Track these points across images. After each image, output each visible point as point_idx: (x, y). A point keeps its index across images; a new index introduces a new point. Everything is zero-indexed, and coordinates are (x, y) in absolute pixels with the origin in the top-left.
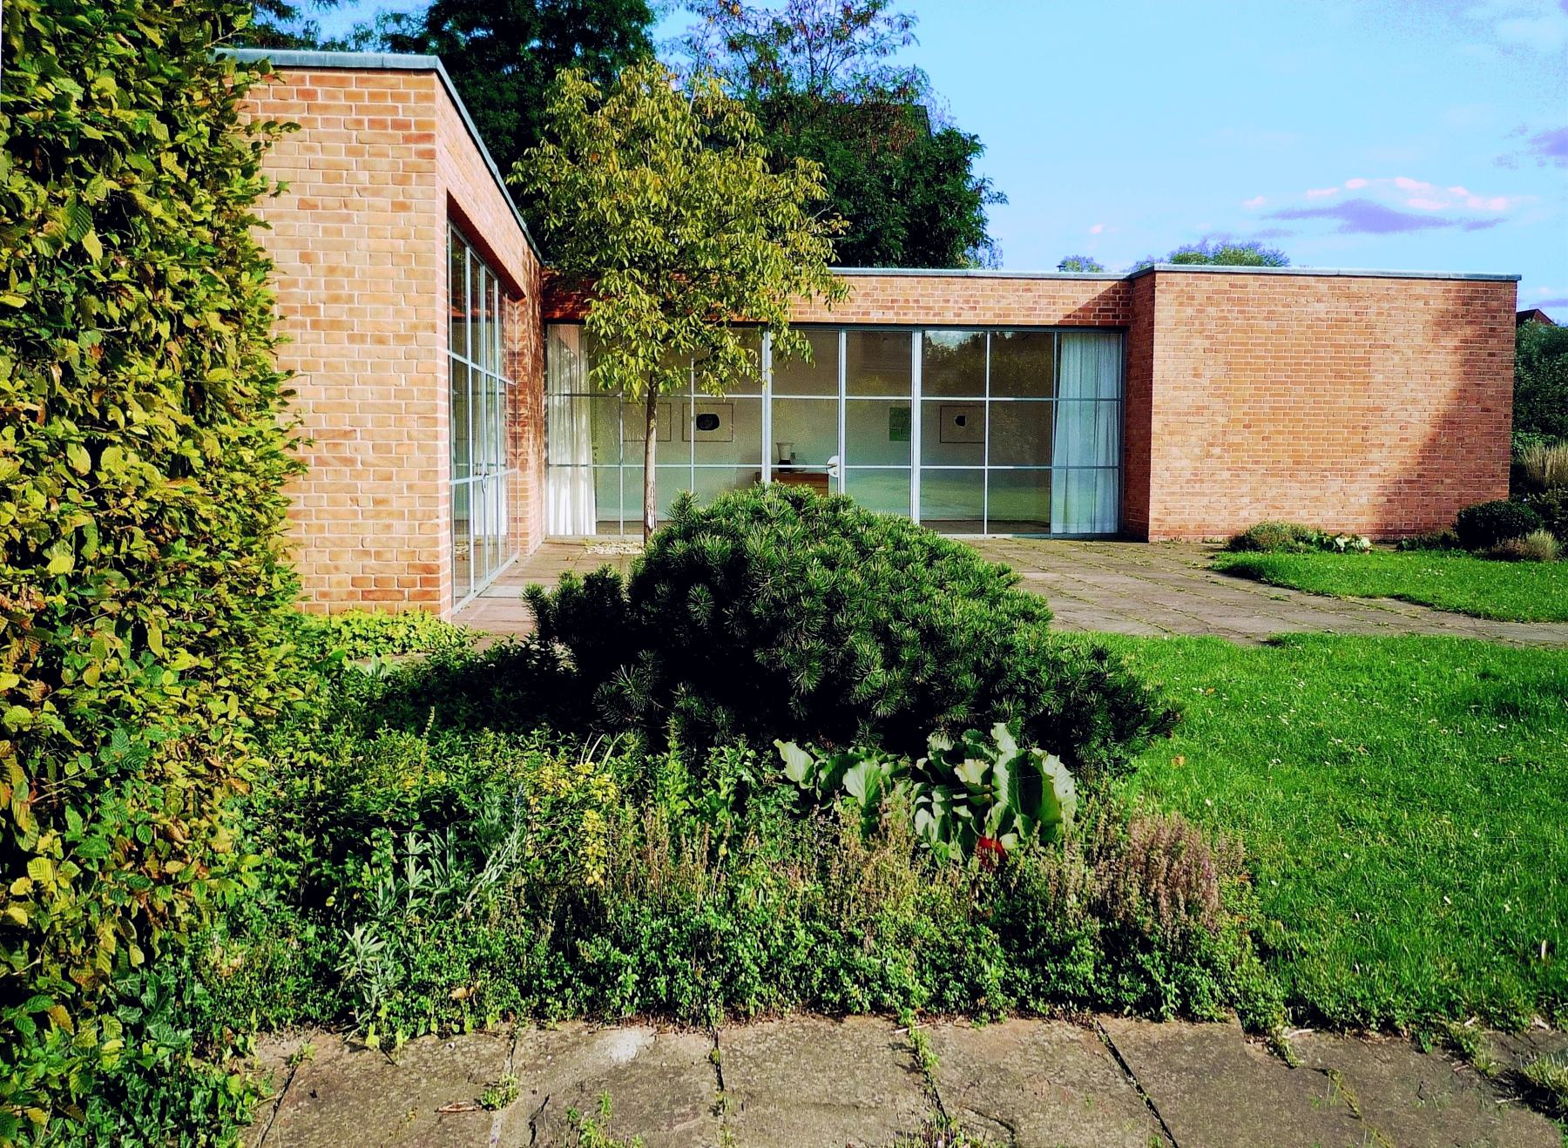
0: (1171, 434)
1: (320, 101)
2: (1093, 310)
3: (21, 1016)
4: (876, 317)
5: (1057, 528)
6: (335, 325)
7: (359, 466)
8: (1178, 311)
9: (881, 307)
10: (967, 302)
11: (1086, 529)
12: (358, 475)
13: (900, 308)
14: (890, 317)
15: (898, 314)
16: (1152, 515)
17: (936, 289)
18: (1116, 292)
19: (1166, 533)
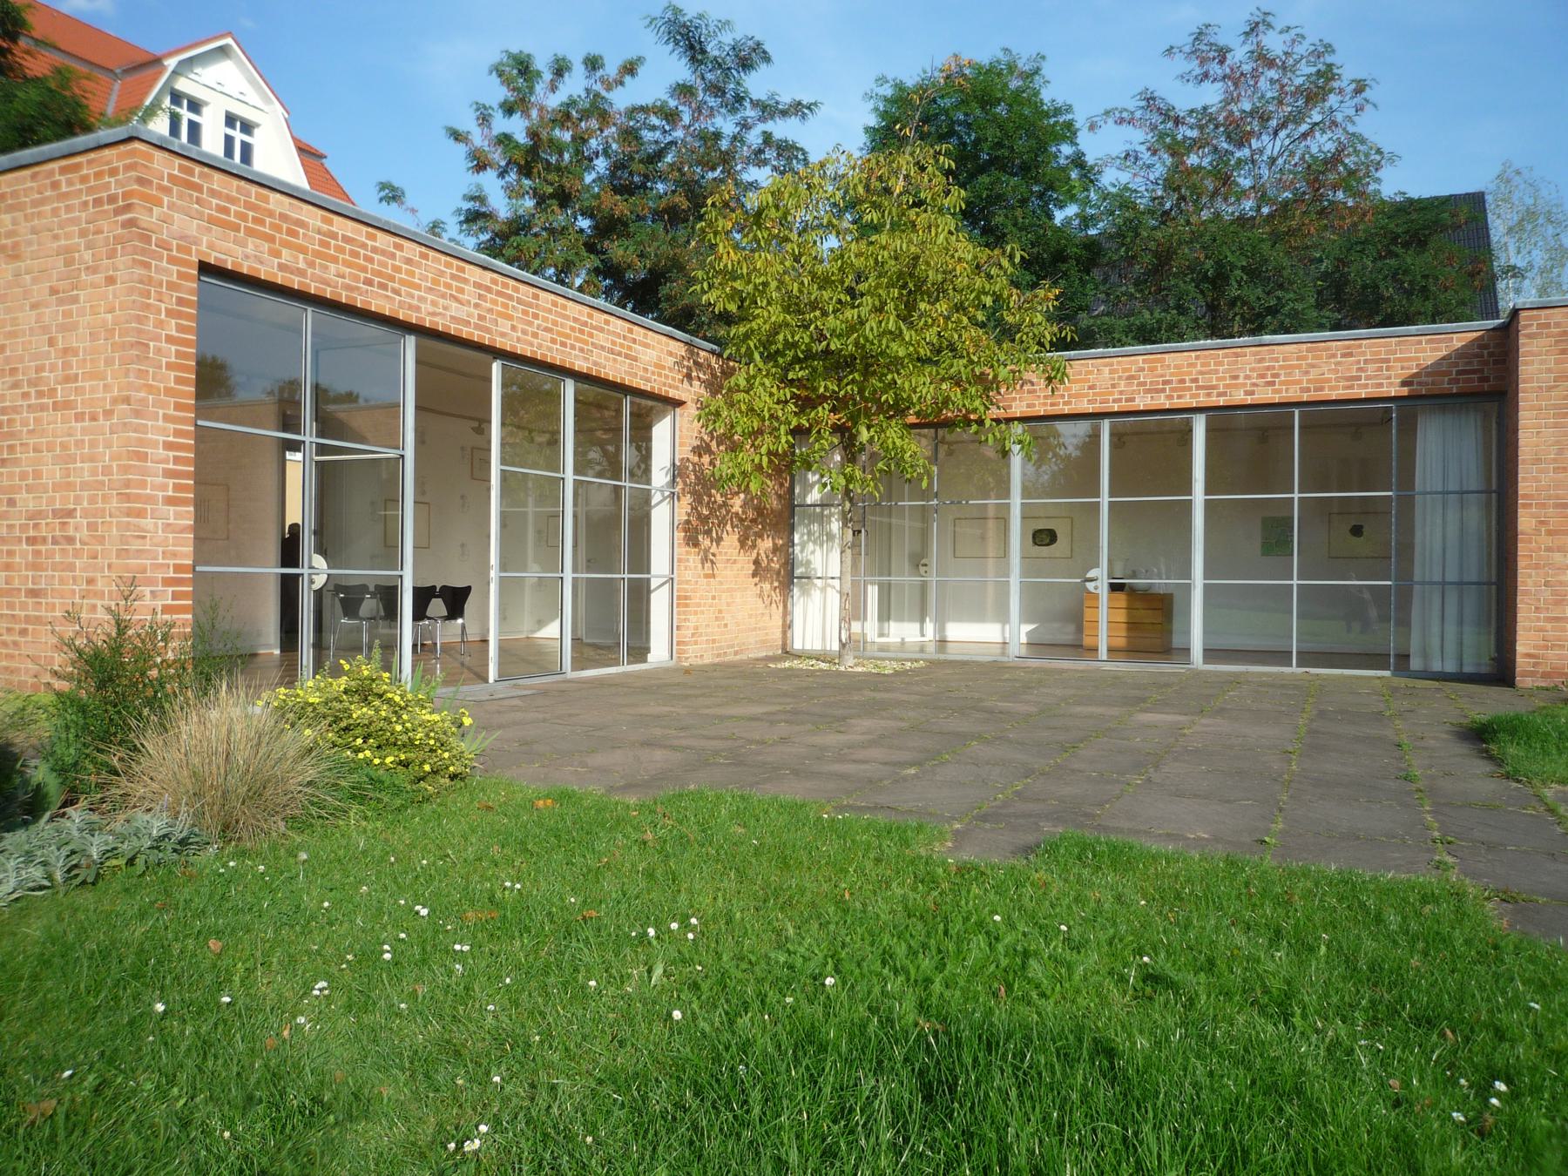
0: (1549, 533)
1: (64, 189)
2: (1448, 373)
3: (1271, 1149)
4: (1141, 403)
5: (1416, 664)
6: (67, 405)
7: (78, 546)
8: (1557, 362)
9: (1149, 391)
10: (1262, 376)
11: (1450, 667)
12: (77, 554)
13: (1172, 390)
14: (1162, 402)
15: (1170, 397)
16: (1520, 649)
17: (1221, 364)
18: (1485, 347)
19: (1545, 675)
